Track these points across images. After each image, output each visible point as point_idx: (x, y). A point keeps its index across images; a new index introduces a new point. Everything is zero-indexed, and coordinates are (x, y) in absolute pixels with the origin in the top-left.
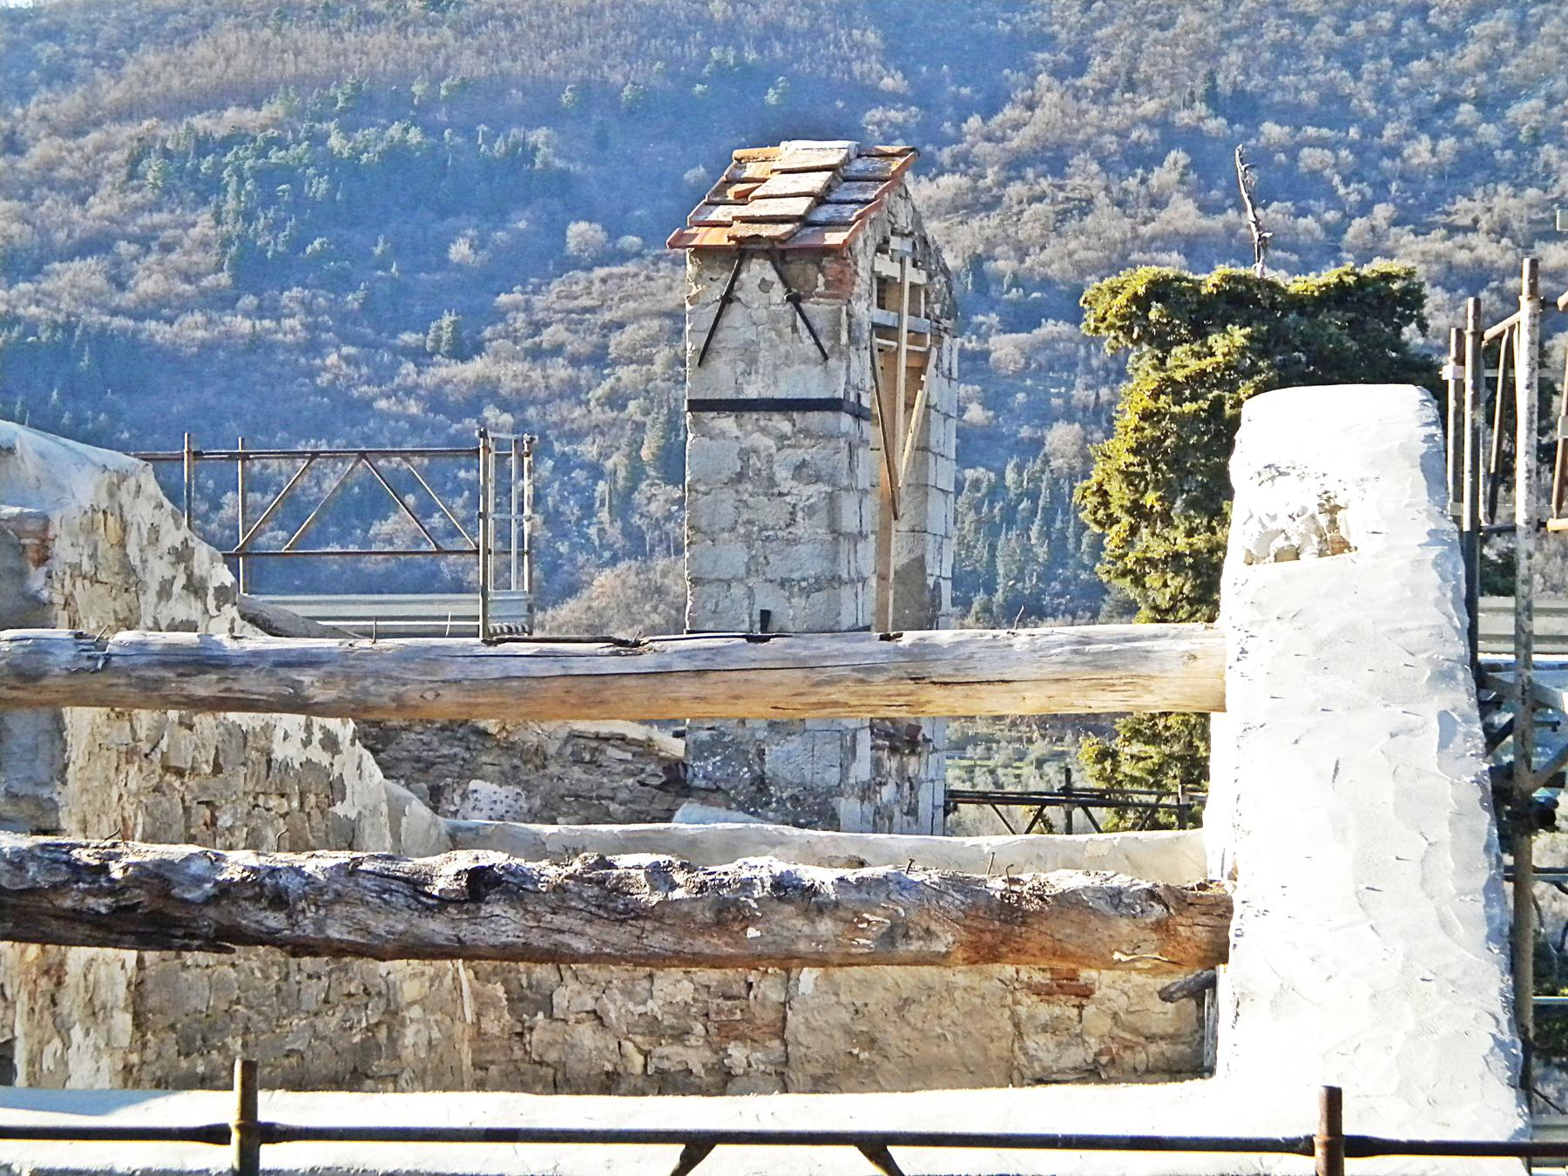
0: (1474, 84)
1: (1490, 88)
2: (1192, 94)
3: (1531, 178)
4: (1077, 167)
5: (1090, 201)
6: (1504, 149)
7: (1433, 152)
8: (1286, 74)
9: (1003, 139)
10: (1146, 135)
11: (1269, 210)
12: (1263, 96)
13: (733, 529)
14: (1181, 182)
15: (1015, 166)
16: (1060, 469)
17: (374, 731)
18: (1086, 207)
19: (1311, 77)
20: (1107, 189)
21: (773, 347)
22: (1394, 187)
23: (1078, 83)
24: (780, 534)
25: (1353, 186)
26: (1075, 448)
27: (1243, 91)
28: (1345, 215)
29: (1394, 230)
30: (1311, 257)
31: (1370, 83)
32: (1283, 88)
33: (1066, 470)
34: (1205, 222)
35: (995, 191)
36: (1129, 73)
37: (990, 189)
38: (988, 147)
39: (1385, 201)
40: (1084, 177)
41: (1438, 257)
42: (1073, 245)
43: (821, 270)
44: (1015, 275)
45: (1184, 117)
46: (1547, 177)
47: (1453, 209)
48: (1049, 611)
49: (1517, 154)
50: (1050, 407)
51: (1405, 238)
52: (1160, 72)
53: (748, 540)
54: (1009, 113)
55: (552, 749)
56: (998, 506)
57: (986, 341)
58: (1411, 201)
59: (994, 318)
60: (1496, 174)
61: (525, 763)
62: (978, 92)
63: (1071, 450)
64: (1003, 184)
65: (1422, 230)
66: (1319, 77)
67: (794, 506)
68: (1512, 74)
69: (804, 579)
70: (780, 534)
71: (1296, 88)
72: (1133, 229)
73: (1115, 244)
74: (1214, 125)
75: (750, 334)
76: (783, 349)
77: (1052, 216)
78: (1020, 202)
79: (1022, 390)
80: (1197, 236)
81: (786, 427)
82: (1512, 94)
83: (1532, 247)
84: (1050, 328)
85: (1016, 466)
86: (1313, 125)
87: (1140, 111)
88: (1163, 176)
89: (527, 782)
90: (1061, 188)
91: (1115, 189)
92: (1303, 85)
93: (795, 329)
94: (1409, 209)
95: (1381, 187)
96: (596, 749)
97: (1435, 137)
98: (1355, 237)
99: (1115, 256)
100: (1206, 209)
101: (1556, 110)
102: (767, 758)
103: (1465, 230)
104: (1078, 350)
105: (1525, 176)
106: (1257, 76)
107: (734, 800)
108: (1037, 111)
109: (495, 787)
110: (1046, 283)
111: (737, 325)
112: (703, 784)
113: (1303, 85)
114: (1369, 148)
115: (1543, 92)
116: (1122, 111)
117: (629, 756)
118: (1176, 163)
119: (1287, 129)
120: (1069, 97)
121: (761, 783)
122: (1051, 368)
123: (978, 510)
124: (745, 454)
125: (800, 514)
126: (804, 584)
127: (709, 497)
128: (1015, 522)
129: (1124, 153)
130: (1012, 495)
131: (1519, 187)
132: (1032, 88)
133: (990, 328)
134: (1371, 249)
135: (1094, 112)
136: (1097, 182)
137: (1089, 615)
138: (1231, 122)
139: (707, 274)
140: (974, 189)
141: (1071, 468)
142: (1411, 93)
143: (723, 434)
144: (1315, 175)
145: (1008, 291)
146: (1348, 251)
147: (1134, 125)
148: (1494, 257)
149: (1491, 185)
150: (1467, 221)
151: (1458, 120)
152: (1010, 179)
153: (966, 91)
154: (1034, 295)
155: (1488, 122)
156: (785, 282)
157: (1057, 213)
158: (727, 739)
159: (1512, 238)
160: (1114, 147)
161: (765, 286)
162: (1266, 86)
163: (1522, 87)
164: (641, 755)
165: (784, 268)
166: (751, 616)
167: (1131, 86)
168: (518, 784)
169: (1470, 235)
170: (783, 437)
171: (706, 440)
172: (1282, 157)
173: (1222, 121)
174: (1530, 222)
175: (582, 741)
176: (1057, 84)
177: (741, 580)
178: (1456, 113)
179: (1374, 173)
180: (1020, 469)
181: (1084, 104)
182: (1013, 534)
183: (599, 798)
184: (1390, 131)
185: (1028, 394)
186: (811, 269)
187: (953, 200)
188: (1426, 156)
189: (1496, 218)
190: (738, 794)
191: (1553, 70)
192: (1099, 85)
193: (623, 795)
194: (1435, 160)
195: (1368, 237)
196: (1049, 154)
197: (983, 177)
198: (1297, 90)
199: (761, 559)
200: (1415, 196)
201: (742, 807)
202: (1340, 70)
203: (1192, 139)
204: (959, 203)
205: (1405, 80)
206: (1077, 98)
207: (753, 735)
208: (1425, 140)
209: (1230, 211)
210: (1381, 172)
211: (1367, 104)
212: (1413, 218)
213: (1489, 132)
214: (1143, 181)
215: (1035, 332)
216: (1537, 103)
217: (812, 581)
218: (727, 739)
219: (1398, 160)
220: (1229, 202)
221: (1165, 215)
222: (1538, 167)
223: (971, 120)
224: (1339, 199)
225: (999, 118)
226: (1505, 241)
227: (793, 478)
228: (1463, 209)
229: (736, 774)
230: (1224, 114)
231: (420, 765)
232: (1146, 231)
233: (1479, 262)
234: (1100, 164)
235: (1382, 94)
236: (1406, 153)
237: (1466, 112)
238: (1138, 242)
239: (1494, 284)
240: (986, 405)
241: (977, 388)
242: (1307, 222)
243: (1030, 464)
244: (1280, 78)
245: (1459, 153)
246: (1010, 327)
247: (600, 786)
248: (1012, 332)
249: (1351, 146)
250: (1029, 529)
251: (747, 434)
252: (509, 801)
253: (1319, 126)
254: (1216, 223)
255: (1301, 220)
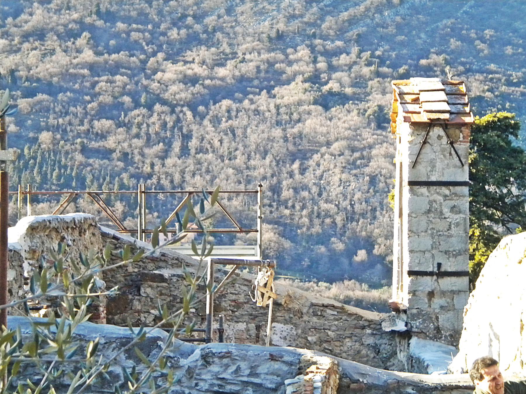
0: (192, 10)
1: (198, 12)
2: (91, 11)
3: (213, 44)
4: (49, 38)
5: (54, 50)
6: (203, 34)
7: (178, 34)
8: (125, 5)
9: (21, 26)
10: (74, 26)
11: (120, 54)
12: (117, 13)
13: (426, 231)
14: (88, 44)
15: (26, 37)
16: (45, 148)
17: (233, 304)
18: (52, 52)
19: (134, 6)
20: (60, 46)
21: (442, 161)
22: (164, 47)
23: (49, 6)
24: (445, 233)
25: (150, 46)
26: (50, 141)
27: (110, 11)
28: (147, 57)
29: (165, 62)
30: (136, 72)
31: (155, 9)
32: (124, 10)
33: (47, 149)
34: (97, 59)
35: (18, 46)
36: (68, 3)
37: (16, 45)
38: (15, 29)
39: (161, 51)
40: (52, 42)
41: (181, 72)
42: (48, 66)
43: (461, 132)
44: (27, 77)
45: (88, 20)
46: (218, 44)
47: (186, 55)
48: (41, 200)
49: (208, 35)
50: (40, 125)
51: (169, 66)
52: (79, 3)
53: (432, 236)
54: (23, 17)
55: (305, 310)
56: (22, 162)
57: (16, 101)
58: (170, 52)
59: (19, 93)
60: (200, 43)
61: (295, 316)
62: (11, 8)
63: (48, 141)
64: (21, 43)
65: (175, 62)
66: (137, 6)
67: (450, 223)
68: (205, 7)
69: (454, 251)
70: (445, 233)
71: (129, 10)
72: (70, 61)
73: (63, 66)
74: (100, 23)
75: (433, 156)
76: (446, 162)
77: (40, 55)
78: (28, 50)
79: (30, 119)
80: (93, 63)
81: (447, 192)
82: (205, 14)
83: (213, 69)
84: (40, 96)
85: (28, 147)
86: (135, 24)
87: (72, 17)
88: (81, 41)
89: (295, 323)
90: (43, 45)
91: (63, 46)
92: (131, 9)
93: (450, 154)
94: (170, 55)
95: (160, 47)
96: (322, 310)
97: (179, 29)
98: (151, 65)
99: (64, 70)
100: (98, 54)
101: (221, 20)
102: (440, 320)
103: (190, 62)
104: (50, 105)
105: (211, 43)
106: (115, 6)
107: (428, 336)
108: (34, 16)
109: (282, 325)
110: (38, 80)
111: (428, 152)
112: (416, 330)
113: (131, 9)
114: (156, 32)
115: (216, 13)
116: (65, 17)
117: (336, 313)
118: (85, 36)
119: (126, 25)
120: (45, 12)
121: (438, 329)
122: (41, 112)
123: (14, 164)
124: (431, 203)
125: (453, 226)
126: (454, 253)
127: (417, 219)
128: (28, 168)
129: (66, 33)
130: (27, 158)
131: (209, 47)
132: (32, 8)
133: (18, 96)
134: (157, 69)
135: (55, 18)
136: (56, 43)
137: (56, 202)
138: (105, 23)
139: (416, 133)
140: (10, 45)
141: (49, 148)
142: (170, 13)
143: (422, 195)
144: (136, 42)
145: (24, 83)
146: (149, 70)
147: (70, 22)
148: (201, 72)
149: (199, 47)
150: (191, 59)
151: (187, 23)
152: (24, 42)
153: (6, 8)
154: (34, 84)
155: (197, 24)
156: (448, 137)
157: (42, 54)
158: (423, 313)
159: (207, 65)
160: (62, 30)
161: (439, 137)
162: (118, 10)
163: (209, 11)
164: (341, 312)
165: (447, 130)
166: (433, 265)
167: (69, 8)
168: (292, 324)
169: (192, 64)
170: (446, 196)
171: (416, 197)
172: (124, 35)
173: (102, 21)
174: (213, 60)
175: (317, 307)
176: (41, 6)
177: (430, 251)
178: (186, 20)
179: (157, 41)
180: (29, 149)
181: (51, 14)
182: (28, 171)
183: (324, 329)
184: (163, 26)
185: (32, 121)
186: (457, 131)
187: (3, 49)
188: (176, 36)
189: (201, 58)
190: (430, 334)
191: (220, 6)
192: (56, 8)
193: (334, 328)
194: (179, 37)
195: (156, 64)
196: (38, 33)
197: (13, 40)
198: (129, 11)
199: (438, 243)
200: (172, 50)
201: (431, 338)
202: (145, 4)
203: (91, 28)
204: (5, 50)
205: (168, 8)
206: (48, 12)
207: (434, 311)
208: (175, 30)
209: (105, 55)
210: (160, 41)
211: (154, 17)
212: (172, 58)
213: (198, 27)
214: (74, 43)
215: (35, 98)
216: (214, 17)
217: (457, 251)
218: (423, 313)
219: (166, 37)
220: (105, 51)
221: (82, 56)
222: (215, 40)
223: (9, 19)
224: (145, 50)
225: (19, 19)
226: (204, 67)
227: (450, 212)
228: (189, 55)
229: (428, 326)
230: (103, 19)
231: (252, 317)
232: (75, 61)
233: (195, 74)
234: (57, 36)
235: (160, 13)
236: (169, 34)
237: (190, 20)
238: (72, 66)
239: (201, 82)
240: (16, 124)
241: (13, 118)
242: (134, 59)
243: (33, 147)
244: (123, 6)
245: (188, 35)
246: (24, 96)
247: (324, 324)
248: (26, 98)
249: (149, 31)
250: (33, 171)
251: (432, 195)
252: (288, 331)
253: (137, 24)
254: (101, 59)
255: (132, 58)
